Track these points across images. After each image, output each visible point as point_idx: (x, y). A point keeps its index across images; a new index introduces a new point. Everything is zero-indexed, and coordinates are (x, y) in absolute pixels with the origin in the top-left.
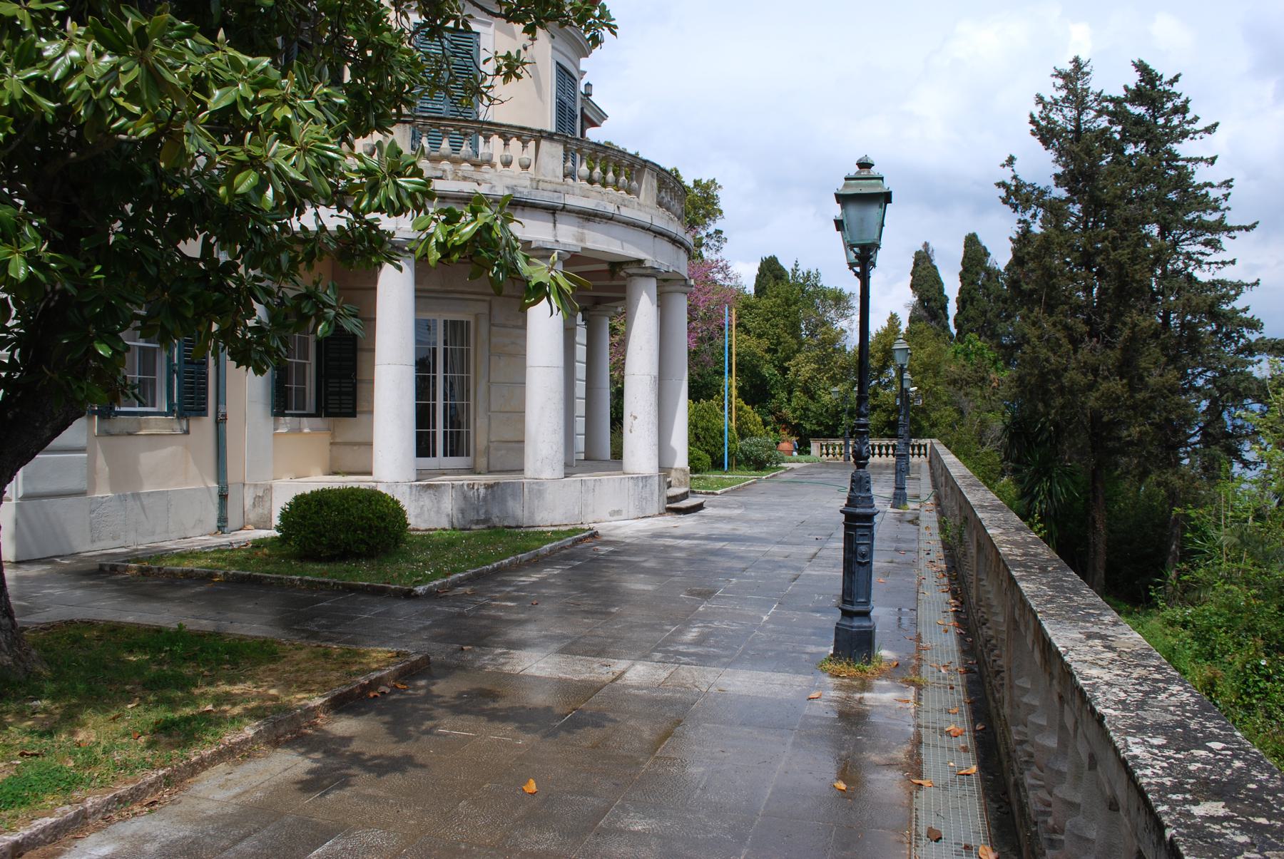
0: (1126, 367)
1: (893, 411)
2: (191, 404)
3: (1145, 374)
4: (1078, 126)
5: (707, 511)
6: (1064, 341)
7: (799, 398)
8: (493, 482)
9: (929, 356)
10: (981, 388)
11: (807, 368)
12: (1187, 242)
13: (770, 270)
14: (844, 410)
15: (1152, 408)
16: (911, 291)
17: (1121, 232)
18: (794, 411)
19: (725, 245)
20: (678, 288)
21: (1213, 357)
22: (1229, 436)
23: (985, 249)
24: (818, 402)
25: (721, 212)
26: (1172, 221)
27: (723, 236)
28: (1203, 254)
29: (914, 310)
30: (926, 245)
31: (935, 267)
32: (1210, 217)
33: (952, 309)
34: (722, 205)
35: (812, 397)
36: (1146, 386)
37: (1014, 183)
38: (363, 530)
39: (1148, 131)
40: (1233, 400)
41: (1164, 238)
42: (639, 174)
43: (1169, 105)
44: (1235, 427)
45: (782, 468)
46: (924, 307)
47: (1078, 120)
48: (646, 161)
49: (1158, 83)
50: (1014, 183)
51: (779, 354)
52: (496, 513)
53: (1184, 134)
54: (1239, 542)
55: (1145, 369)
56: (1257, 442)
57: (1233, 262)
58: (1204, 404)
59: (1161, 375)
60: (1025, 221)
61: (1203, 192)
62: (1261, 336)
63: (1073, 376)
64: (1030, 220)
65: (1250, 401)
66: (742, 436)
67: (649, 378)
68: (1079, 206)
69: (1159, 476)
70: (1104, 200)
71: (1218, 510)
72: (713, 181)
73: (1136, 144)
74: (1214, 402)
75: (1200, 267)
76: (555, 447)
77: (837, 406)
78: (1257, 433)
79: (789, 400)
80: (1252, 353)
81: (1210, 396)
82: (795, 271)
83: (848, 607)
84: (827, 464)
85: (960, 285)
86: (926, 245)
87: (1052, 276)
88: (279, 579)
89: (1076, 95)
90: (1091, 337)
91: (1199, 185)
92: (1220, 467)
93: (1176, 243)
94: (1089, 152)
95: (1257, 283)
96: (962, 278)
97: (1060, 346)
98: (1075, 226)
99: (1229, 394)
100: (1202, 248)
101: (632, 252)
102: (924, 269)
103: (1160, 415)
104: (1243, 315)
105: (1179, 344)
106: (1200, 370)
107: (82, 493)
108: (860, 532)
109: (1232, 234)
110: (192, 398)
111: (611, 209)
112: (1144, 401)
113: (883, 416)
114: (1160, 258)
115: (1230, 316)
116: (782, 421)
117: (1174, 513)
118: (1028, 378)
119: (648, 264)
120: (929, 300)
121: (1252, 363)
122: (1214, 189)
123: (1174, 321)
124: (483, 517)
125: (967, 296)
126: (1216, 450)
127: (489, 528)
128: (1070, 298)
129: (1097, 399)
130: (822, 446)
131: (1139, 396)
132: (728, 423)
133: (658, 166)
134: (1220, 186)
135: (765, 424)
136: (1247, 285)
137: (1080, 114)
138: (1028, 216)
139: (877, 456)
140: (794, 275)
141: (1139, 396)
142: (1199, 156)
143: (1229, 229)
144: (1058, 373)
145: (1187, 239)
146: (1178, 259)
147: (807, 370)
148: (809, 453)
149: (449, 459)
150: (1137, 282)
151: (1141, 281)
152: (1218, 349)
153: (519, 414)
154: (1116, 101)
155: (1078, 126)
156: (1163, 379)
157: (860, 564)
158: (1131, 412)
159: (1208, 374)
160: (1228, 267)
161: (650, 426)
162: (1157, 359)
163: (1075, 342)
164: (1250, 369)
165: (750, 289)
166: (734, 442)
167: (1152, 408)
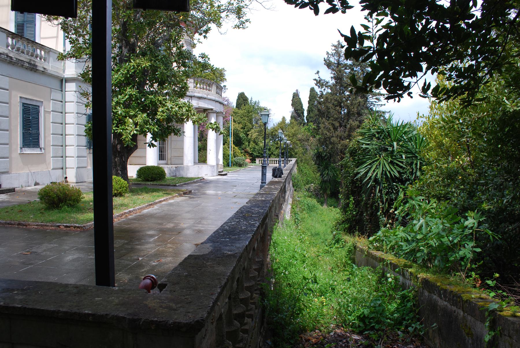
6: (332, 129)
9: (295, 131)
10: (308, 142)
13: (242, 99)
18: (251, 149)
19: (227, 91)
20: (220, 115)
25: (226, 80)
27: (226, 87)
29: (293, 113)
30: (297, 90)
31: (300, 99)
33: (306, 114)
34: (226, 77)
46: (296, 112)
52: (178, 174)
60: (322, 91)
63: (334, 139)
64: (323, 91)
66: (235, 157)
72: (223, 69)
79: (249, 145)
82: (251, 101)
85: (308, 105)
86: (297, 90)
96: (309, 103)
100: (376, 100)
101: (210, 107)
107: (86, 167)
111: (205, 96)
116: (246, 152)
119: (214, 110)
120: (298, 110)
125: (310, 109)
132: (231, 153)
135: (242, 153)
137: (339, 58)
138: (322, 90)
140: (251, 102)
144: (330, 138)
147: (255, 135)
148: (255, 163)
153: (182, 149)
163: (335, 129)
165: (234, 104)
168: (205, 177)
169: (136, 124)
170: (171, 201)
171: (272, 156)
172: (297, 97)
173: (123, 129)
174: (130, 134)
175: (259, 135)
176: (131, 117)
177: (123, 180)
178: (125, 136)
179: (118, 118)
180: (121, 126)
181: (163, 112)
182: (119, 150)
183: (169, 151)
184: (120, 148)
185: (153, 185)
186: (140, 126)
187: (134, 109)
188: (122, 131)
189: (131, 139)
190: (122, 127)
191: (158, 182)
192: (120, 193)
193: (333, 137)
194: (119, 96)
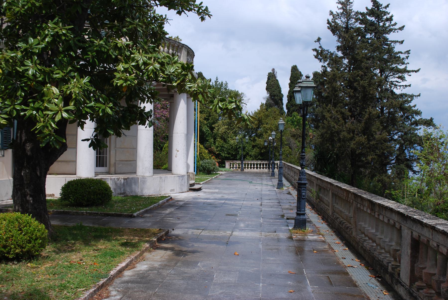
0: (366, 131)
1: (263, 148)
2: (5, 144)
3: (374, 133)
4: (347, 26)
5: (204, 190)
7: (219, 142)
8: (126, 177)
11: (223, 128)
12: (391, 77)
14: (240, 147)
15: (376, 148)
16: (266, 91)
17: (365, 73)
21: (401, 126)
22: (408, 160)
23: (300, 73)
24: (229, 143)
26: (386, 68)
28: (397, 82)
30: (273, 70)
31: (277, 80)
32: (401, 67)
33: (285, 101)
35: (225, 140)
36: (374, 139)
37: (320, 49)
38: (99, 194)
39: (376, 28)
40: (409, 145)
41: (381, 75)
42: (181, 49)
43: (385, 17)
44: (410, 156)
45: (218, 174)
46: (272, 99)
47: (347, 23)
48: (183, 45)
49: (380, 7)
50: (320, 49)
51: (210, 121)
52: (128, 190)
53: (391, 30)
54: (412, 203)
55: (374, 131)
56: (419, 163)
57: (410, 86)
58: (398, 146)
59: (380, 134)
60: (324, 66)
61: (398, 55)
62: (421, 117)
65: (416, 145)
67: (184, 135)
68: (347, 60)
69: (380, 177)
70: (358, 59)
71: (403, 192)
73: (371, 34)
74: (401, 146)
75: (396, 87)
76: (150, 163)
77: (237, 145)
78: (419, 159)
79: (215, 143)
80: (417, 125)
81: (400, 143)
83: (299, 212)
84: (233, 172)
85: (289, 89)
86: (273, 70)
87: (336, 91)
88: (77, 212)
89: (347, 12)
90: (351, 117)
91: (396, 52)
92: (404, 173)
93: (386, 77)
94: (352, 38)
95: (419, 95)
97: (339, 121)
98: (345, 69)
99: (408, 142)
100: (397, 80)
102: (272, 81)
103: (380, 151)
104: (413, 108)
105: (388, 121)
106: (396, 132)
108: (303, 189)
109: (410, 74)
110: (6, 141)
112: (373, 145)
113: (258, 150)
114: (380, 84)
115: (408, 109)
117: (386, 192)
118: (326, 134)
120: (274, 96)
121: (417, 129)
122: (403, 54)
123: (386, 111)
124: (122, 192)
126: (402, 166)
127: (125, 196)
128: (343, 100)
129: (354, 144)
130: (230, 164)
131: (372, 143)
133: (188, 46)
134: (405, 53)
136: (416, 96)
137: (348, 20)
139: (255, 169)
141: (372, 143)
142: (397, 40)
143: (409, 72)
144: (338, 133)
145: (391, 75)
146: (387, 84)
147: (223, 129)
148: (225, 167)
149: (98, 168)
150: (371, 94)
151: (373, 94)
152: (403, 123)
154: (362, 14)
155: (347, 26)
156: (382, 136)
157: (303, 199)
158: (368, 150)
159: (399, 133)
160: (408, 88)
161: (184, 155)
162: (379, 127)
164: (416, 132)
166: (199, 162)
167: (376, 148)
168: (173, 195)
169: (67, 99)
170: (142, 267)
171: (248, 157)
172: (274, 79)
173: (38, 110)
174: (53, 119)
175: (228, 129)
176: (57, 83)
177: (35, 223)
178: (42, 124)
179: (27, 85)
180: (34, 103)
181: (126, 70)
182: (29, 153)
183: (113, 152)
184: (32, 150)
185: (90, 214)
186: (77, 103)
187: (61, 66)
188: (35, 112)
189: (56, 131)
190: (37, 105)
191: (100, 208)
192: (28, 252)
193: (344, 131)
194: (31, 40)
